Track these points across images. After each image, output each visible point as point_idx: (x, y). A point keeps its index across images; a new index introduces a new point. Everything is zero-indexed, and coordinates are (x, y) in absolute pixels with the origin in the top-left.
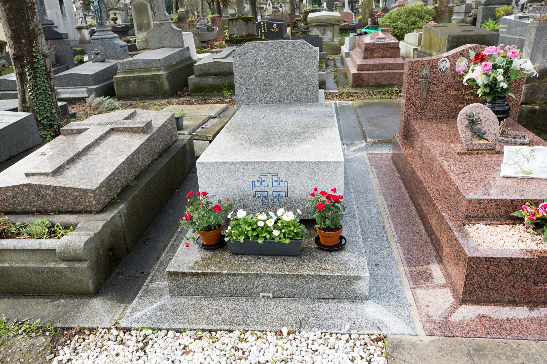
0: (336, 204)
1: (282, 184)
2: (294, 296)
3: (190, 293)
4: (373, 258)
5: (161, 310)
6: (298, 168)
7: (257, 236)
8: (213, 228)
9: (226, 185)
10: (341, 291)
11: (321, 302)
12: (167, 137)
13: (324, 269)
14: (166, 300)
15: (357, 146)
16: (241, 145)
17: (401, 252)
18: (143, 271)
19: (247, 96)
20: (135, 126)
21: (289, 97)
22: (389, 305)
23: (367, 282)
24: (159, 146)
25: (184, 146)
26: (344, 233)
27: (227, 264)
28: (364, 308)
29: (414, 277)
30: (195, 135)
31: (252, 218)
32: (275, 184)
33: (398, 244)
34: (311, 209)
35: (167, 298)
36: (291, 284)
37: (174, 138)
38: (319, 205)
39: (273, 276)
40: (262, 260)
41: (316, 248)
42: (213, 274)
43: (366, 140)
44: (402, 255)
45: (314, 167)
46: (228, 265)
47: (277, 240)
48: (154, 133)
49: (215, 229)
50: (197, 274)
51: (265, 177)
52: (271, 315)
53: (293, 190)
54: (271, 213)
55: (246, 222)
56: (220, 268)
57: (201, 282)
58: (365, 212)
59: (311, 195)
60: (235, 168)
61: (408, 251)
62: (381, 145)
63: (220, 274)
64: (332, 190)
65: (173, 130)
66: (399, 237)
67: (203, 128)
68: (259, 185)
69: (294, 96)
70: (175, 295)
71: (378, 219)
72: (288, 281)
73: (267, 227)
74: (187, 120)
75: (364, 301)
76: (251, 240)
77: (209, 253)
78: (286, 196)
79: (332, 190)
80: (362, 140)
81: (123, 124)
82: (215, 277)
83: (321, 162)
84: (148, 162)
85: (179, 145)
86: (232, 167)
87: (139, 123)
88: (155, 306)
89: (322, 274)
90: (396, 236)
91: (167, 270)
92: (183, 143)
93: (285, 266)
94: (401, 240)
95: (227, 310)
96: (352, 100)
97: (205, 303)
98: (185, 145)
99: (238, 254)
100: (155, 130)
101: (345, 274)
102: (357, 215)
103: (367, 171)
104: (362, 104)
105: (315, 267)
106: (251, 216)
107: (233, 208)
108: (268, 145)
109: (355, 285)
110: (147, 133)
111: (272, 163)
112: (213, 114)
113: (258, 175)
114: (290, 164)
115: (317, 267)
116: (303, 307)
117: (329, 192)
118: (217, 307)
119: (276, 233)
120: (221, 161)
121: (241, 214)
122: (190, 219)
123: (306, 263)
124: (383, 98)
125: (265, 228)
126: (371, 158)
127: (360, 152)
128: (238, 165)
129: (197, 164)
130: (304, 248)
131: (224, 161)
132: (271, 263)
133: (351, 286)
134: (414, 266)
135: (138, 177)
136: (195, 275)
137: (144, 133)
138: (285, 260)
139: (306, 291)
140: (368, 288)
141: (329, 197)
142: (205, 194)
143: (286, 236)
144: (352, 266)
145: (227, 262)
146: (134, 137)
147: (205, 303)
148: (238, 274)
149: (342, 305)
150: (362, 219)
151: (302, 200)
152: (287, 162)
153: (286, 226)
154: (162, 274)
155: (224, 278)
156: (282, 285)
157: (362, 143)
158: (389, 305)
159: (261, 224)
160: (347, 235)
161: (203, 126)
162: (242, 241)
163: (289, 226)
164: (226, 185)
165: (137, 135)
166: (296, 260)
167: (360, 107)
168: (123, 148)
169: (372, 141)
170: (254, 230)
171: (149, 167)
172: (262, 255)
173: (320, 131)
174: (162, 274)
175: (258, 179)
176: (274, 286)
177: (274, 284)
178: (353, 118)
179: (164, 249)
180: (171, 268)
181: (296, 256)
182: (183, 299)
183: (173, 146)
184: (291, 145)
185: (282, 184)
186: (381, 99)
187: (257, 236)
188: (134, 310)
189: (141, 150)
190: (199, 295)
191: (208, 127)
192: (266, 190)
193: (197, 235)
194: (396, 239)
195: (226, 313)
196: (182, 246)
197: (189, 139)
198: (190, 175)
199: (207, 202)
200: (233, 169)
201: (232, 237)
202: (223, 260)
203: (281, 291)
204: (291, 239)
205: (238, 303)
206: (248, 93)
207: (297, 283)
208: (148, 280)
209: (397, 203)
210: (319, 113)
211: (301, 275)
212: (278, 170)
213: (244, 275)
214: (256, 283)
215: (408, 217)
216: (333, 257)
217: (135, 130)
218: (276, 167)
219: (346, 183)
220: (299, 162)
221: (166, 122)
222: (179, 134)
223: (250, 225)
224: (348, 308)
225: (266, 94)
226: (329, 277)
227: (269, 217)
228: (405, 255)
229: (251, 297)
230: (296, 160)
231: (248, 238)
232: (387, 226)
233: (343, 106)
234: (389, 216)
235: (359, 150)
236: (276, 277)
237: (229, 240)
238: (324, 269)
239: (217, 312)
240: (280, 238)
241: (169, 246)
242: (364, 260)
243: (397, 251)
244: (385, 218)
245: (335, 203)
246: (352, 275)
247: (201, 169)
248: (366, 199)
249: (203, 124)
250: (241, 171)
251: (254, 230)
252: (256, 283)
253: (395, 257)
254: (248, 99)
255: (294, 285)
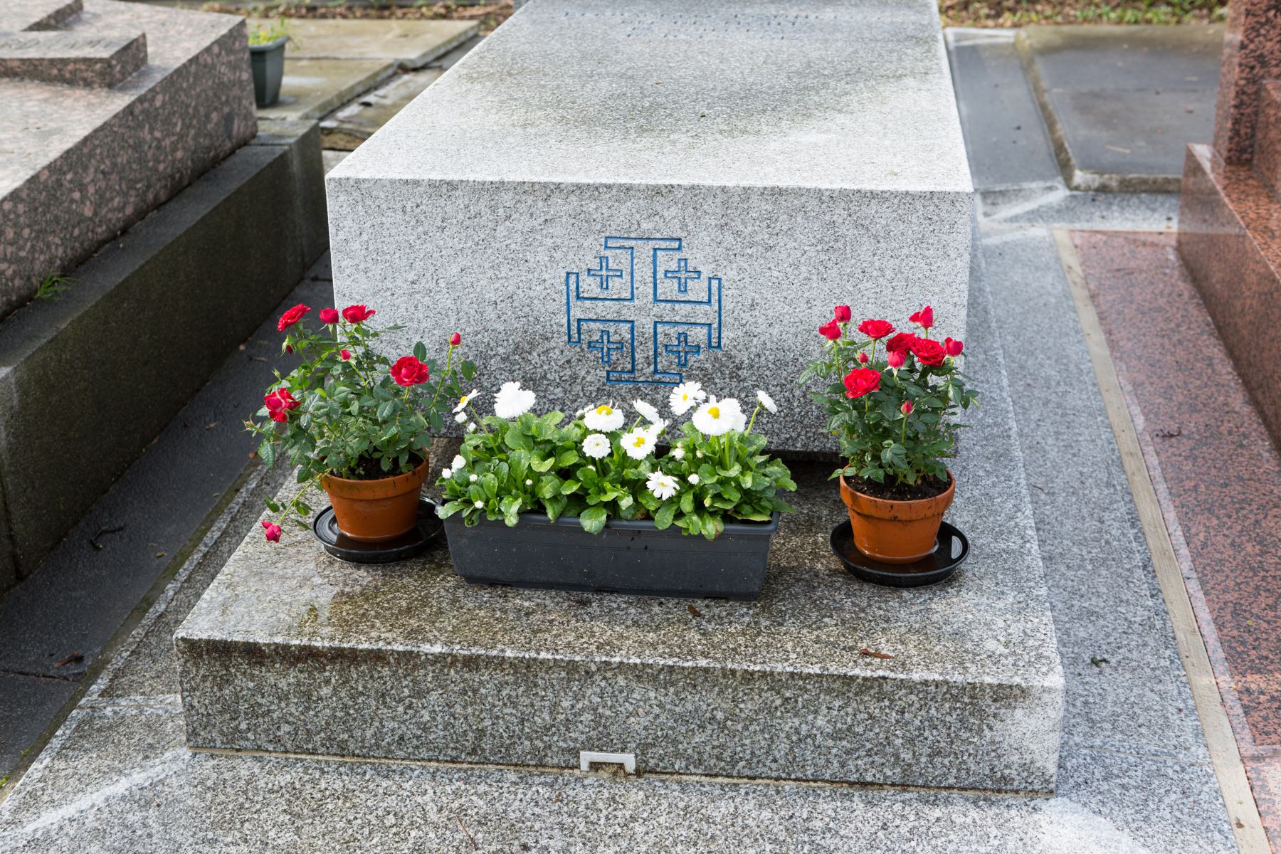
0: (932, 379)
1: (697, 290)
2: (728, 769)
3: (278, 740)
4: (1082, 634)
5: (148, 803)
6: (770, 220)
7: (579, 501)
8: (386, 466)
9: (451, 286)
10: (936, 753)
11: (849, 797)
12: (207, 116)
13: (865, 654)
14: (174, 764)
15: (1027, 198)
16: (524, 126)
17: (1205, 615)
18: (79, 652)
20: (73, 54)
22: (1146, 819)
23: (1056, 712)
24: (175, 149)
25: (282, 160)
26: (958, 516)
27: (442, 620)
28: (1037, 826)
29: (1256, 716)
30: (330, 131)
31: (560, 426)
32: (668, 288)
33: (1194, 586)
34: (821, 395)
35: (175, 759)
36: (720, 715)
37: (238, 127)
38: (857, 374)
39: (639, 673)
40: (594, 608)
41: (834, 573)
42: (378, 657)
44: (1210, 631)
45: (839, 215)
46: (447, 623)
47: (664, 520)
48: (152, 90)
49: (395, 469)
50: (308, 655)
51: (625, 256)
52: (624, 844)
53: (746, 316)
54: (643, 408)
55: (532, 441)
56: (412, 634)
57: (325, 691)
58: (1053, 454)
59: (823, 331)
60: (494, 209)
61: (1235, 613)
62: (1134, 200)
63: (408, 658)
64: (914, 318)
65: (236, 91)
66: (1196, 556)
67: (367, 105)
68: (596, 292)
70: (209, 745)
71: (1108, 485)
72: (709, 701)
73: (626, 461)
74: (295, 72)
75: (1038, 802)
76: (550, 515)
77: (364, 576)
78: (714, 345)
79: (914, 318)
80: (1053, 177)
81: (22, 46)
82: (386, 671)
83: (874, 195)
84: (121, 209)
85: (259, 157)
86: (482, 206)
87: (92, 43)
88: (121, 786)
89: (857, 671)
90: (1184, 551)
91: (180, 633)
92: (279, 151)
93: (694, 636)
94: (1207, 570)
95: (433, 816)
96: (1015, 26)
97: (338, 785)
98: (283, 156)
99: (493, 583)
100: (158, 77)
101: (957, 678)
102: (1018, 454)
103: (1068, 296)
104: (1057, 40)
105: (827, 643)
106: (558, 416)
107: (477, 376)
108: (641, 130)
109: (998, 725)
110: (123, 89)
111: (657, 191)
112: (412, 54)
113: (593, 243)
114: (733, 201)
115: (834, 645)
116: (766, 814)
117: (904, 326)
118: (391, 801)
119: (662, 485)
120: (436, 176)
121: (513, 401)
122: (288, 413)
123: (790, 626)
124: (1149, 22)
125: (616, 468)
126: (1090, 250)
127: (1046, 231)
128: (507, 198)
129: (329, 188)
130: (783, 571)
131: (449, 177)
132: (636, 623)
133: (981, 730)
134: (1259, 671)
135: (79, 264)
136: (298, 659)
137: (110, 86)
138: (696, 614)
139: (782, 747)
140: (1054, 740)
141: (901, 345)
142: (358, 314)
143: (707, 502)
144: (991, 645)
145: (440, 612)
146: (68, 102)
147: (338, 785)
148: (489, 660)
149: (937, 813)
150: (1040, 482)
151: (780, 364)
152: (724, 189)
153: (706, 459)
154: (158, 667)
155: (427, 676)
156: (681, 719)
157: (1050, 189)
158: (1146, 819)
159: (596, 448)
160: (973, 528)
161: (370, 98)
162: (511, 521)
163: (722, 464)
164: (451, 286)
165: (79, 92)
166: (745, 613)
167: (1047, 51)
168: (15, 140)
169: (1092, 179)
170: (565, 474)
171: (124, 231)
172: (599, 590)
173: (872, 89)
174: (158, 667)
175: (595, 265)
176: (645, 721)
177: (644, 710)
178: (1014, 98)
179: (171, 573)
180: (201, 624)
181: (746, 597)
182: (246, 767)
183: (234, 159)
184: (744, 132)
185: (697, 290)
186: (1136, 22)
187: (579, 501)
188: (31, 802)
189: (91, 155)
190: (314, 752)
191: (387, 102)
192: (626, 314)
193: (322, 500)
194: (1186, 565)
195: (429, 828)
196: (252, 544)
197: (305, 137)
198: (302, 291)
199: (368, 354)
200: (487, 216)
201: (469, 502)
202: (424, 602)
203: (675, 742)
204: (727, 517)
205: (482, 788)
207: (747, 707)
208: (101, 683)
209: (1193, 424)
210: (869, 26)
211: (764, 675)
212: (684, 226)
213: (515, 665)
214: (566, 704)
215: (1240, 478)
216: (907, 609)
217: (73, 73)
218: (674, 211)
219: (974, 304)
220: (777, 193)
221: (208, 50)
222: (261, 119)
223: (551, 450)
224: (964, 826)
226: (887, 688)
227: (632, 419)
228: (1220, 627)
229: (541, 765)
230: (760, 184)
231: (539, 507)
232: (1147, 511)
233: (974, 49)
234: (1157, 473)
235: (1034, 216)
236: (655, 678)
237: (456, 517)
238: (865, 654)
239: (391, 820)
240: (680, 515)
241: (197, 557)
242: (1043, 626)
243: (1189, 611)
244: (1140, 484)
245: (924, 374)
246: (988, 680)
247: (346, 209)
248: (1059, 405)
249: (367, 91)
250: (522, 223)
251: (565, 474)
252: (566, 704)
253: (1180, 635)
255: (731, 716)
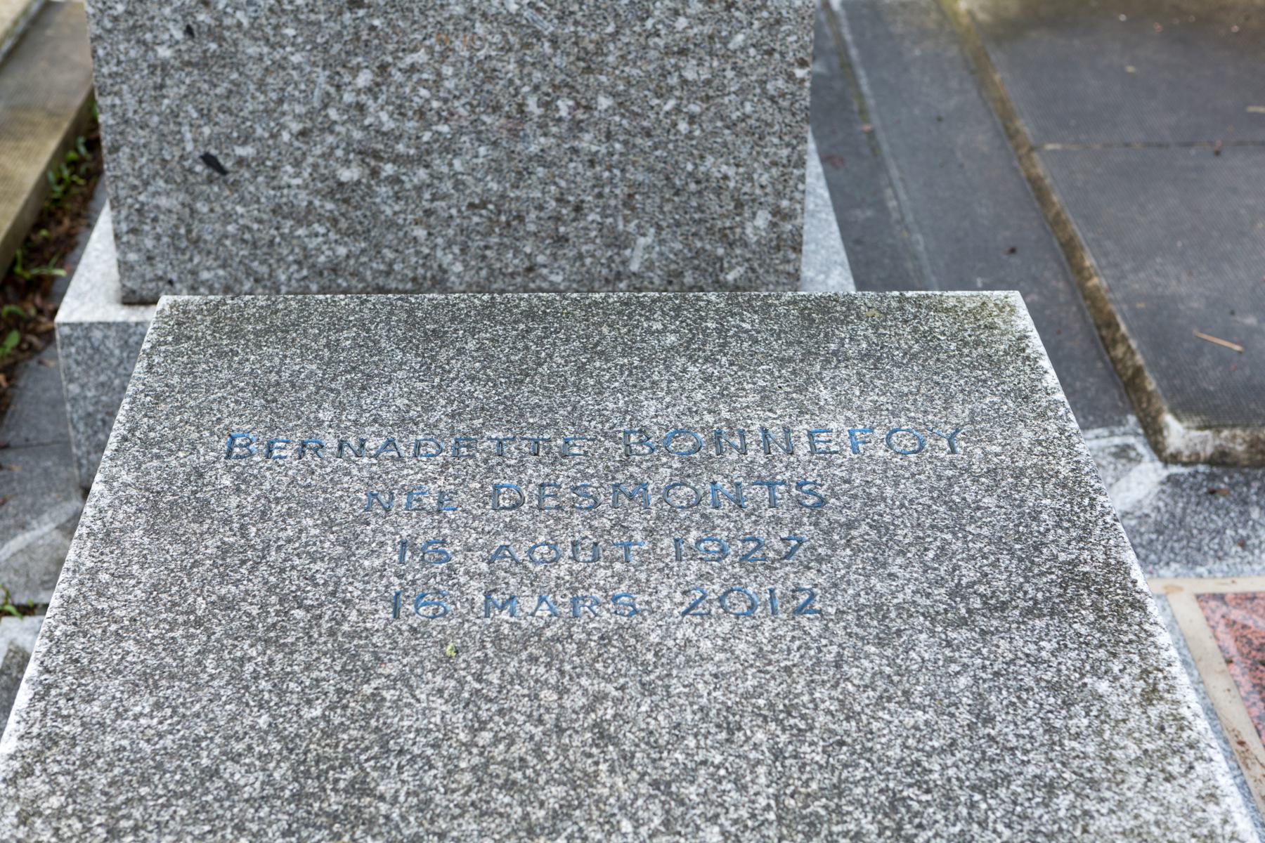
19: (194, 91)
21: (564, 107)
43: (1153, 433)
69: (604, 102)
206: (203, 64)
225: (364, 79)
254: (205, 115)
